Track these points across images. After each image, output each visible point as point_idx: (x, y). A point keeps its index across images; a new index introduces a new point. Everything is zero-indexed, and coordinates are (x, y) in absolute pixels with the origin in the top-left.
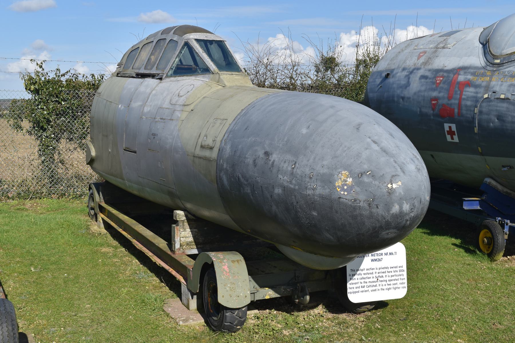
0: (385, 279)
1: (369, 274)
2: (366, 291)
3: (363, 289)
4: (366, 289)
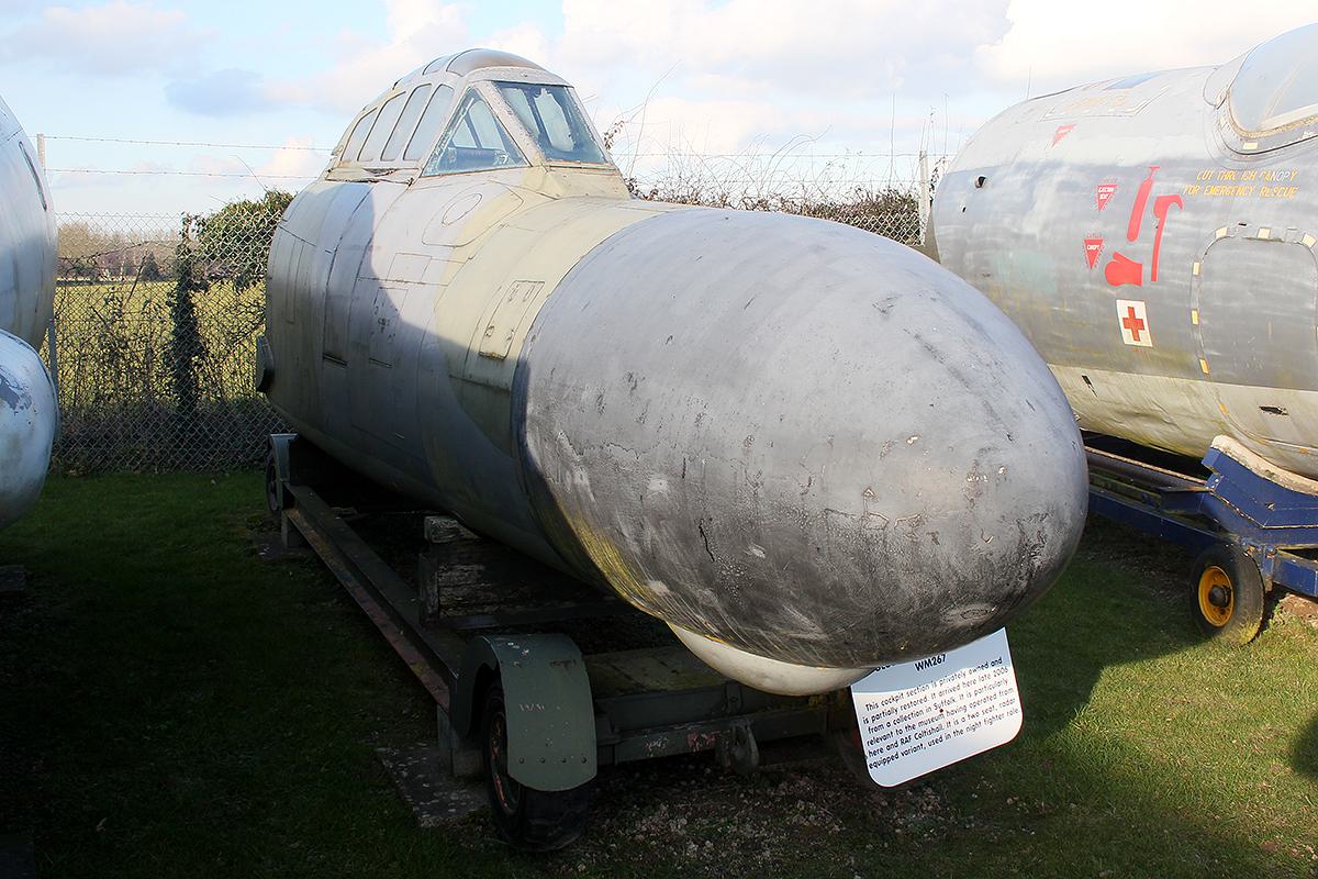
0: (960, 703)
1: (915, 703)
2: (915, 749)
3: (907, 747)
4: (914, 743)
